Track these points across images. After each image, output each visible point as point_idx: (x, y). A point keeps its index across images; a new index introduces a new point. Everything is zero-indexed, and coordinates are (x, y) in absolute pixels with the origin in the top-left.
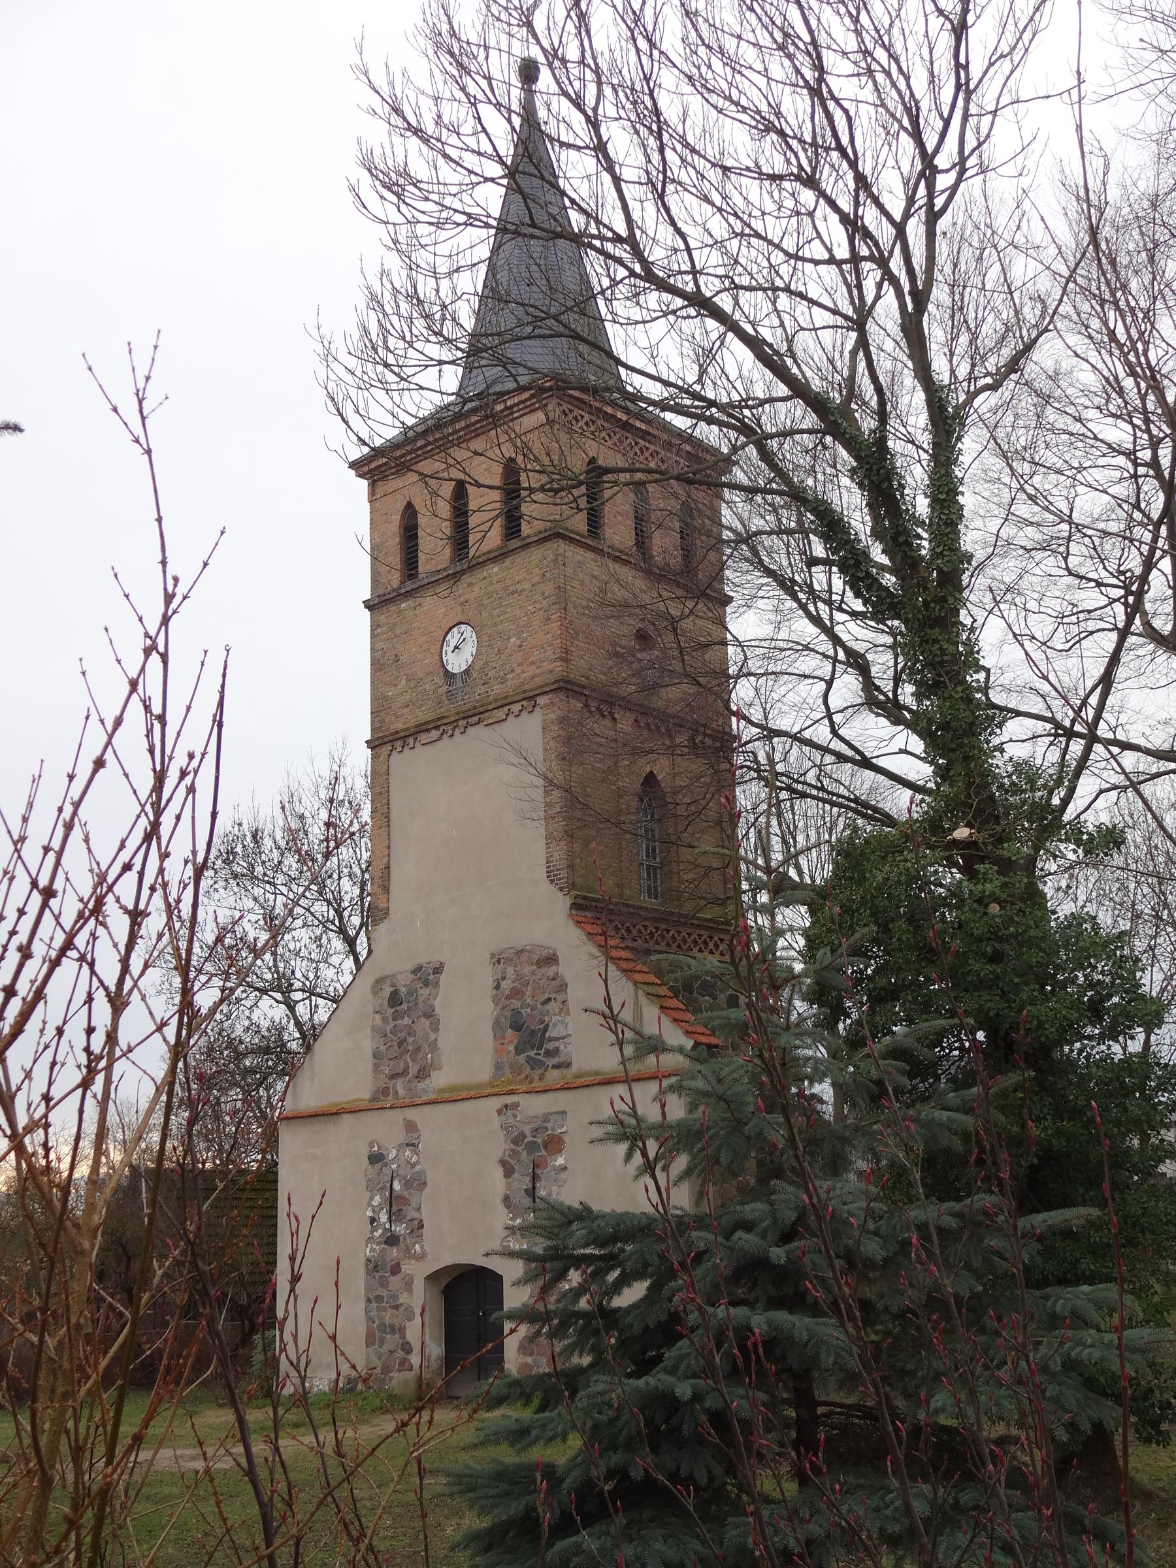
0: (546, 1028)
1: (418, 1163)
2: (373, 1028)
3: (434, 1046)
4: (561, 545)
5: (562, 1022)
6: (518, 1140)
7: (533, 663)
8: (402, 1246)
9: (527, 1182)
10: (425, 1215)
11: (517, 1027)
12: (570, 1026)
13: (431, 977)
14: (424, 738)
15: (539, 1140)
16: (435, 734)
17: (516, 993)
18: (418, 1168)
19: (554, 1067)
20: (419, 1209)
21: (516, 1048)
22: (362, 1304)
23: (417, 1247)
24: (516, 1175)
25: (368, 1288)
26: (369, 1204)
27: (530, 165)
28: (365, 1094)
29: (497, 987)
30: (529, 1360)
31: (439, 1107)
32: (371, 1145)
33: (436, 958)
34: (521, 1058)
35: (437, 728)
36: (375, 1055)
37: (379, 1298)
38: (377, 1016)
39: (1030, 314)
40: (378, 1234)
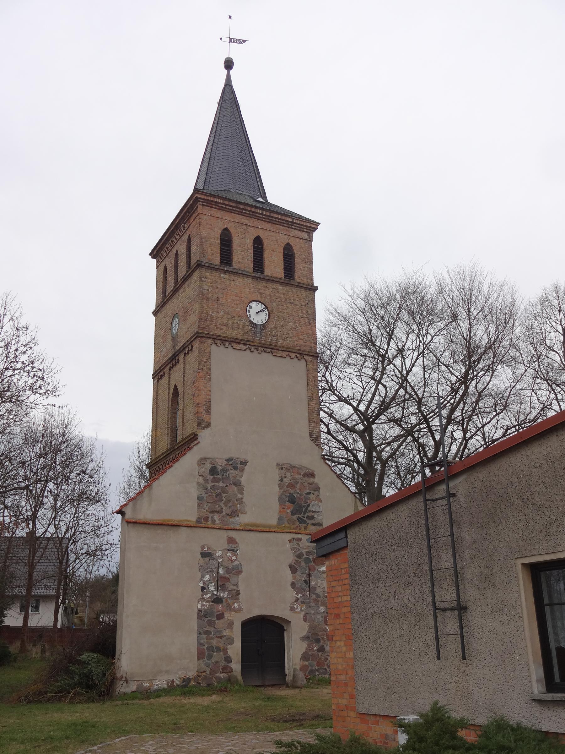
0: (309, 506)
1: (236, 560)
2: (198, 483)
3: (240, 501)
4: (203, 270)
5: (318, 505)
6: (299, 556)
7: (301, 339)
8: (225, 604)
9: (305, 577)
10: (241, 588)
11: (292, 500)
12: (321, 508)
13: (239, 466)
14: (236, 346)
15: (311, 558)
16: (243, 347)
17: (291, 486)
18: (236, 563)
19: (313, 524)
20: (237, 585)
21: (292, 512)
22: (195, 636)
23: (236, 605)
24: (298, 573)
25: (199, 626)
26: (201, 580)
27: (229, 102)
28: (193, 519)
29: (281, 480)
30: (307, 663)
31: (252, 534)
32: (203, 547)
33: (243, 457)
34: (295, 517)
35: (245, 344)
36: (199, 498)
37: (207, 633)
38: (201, 478)
39: (502, 317)
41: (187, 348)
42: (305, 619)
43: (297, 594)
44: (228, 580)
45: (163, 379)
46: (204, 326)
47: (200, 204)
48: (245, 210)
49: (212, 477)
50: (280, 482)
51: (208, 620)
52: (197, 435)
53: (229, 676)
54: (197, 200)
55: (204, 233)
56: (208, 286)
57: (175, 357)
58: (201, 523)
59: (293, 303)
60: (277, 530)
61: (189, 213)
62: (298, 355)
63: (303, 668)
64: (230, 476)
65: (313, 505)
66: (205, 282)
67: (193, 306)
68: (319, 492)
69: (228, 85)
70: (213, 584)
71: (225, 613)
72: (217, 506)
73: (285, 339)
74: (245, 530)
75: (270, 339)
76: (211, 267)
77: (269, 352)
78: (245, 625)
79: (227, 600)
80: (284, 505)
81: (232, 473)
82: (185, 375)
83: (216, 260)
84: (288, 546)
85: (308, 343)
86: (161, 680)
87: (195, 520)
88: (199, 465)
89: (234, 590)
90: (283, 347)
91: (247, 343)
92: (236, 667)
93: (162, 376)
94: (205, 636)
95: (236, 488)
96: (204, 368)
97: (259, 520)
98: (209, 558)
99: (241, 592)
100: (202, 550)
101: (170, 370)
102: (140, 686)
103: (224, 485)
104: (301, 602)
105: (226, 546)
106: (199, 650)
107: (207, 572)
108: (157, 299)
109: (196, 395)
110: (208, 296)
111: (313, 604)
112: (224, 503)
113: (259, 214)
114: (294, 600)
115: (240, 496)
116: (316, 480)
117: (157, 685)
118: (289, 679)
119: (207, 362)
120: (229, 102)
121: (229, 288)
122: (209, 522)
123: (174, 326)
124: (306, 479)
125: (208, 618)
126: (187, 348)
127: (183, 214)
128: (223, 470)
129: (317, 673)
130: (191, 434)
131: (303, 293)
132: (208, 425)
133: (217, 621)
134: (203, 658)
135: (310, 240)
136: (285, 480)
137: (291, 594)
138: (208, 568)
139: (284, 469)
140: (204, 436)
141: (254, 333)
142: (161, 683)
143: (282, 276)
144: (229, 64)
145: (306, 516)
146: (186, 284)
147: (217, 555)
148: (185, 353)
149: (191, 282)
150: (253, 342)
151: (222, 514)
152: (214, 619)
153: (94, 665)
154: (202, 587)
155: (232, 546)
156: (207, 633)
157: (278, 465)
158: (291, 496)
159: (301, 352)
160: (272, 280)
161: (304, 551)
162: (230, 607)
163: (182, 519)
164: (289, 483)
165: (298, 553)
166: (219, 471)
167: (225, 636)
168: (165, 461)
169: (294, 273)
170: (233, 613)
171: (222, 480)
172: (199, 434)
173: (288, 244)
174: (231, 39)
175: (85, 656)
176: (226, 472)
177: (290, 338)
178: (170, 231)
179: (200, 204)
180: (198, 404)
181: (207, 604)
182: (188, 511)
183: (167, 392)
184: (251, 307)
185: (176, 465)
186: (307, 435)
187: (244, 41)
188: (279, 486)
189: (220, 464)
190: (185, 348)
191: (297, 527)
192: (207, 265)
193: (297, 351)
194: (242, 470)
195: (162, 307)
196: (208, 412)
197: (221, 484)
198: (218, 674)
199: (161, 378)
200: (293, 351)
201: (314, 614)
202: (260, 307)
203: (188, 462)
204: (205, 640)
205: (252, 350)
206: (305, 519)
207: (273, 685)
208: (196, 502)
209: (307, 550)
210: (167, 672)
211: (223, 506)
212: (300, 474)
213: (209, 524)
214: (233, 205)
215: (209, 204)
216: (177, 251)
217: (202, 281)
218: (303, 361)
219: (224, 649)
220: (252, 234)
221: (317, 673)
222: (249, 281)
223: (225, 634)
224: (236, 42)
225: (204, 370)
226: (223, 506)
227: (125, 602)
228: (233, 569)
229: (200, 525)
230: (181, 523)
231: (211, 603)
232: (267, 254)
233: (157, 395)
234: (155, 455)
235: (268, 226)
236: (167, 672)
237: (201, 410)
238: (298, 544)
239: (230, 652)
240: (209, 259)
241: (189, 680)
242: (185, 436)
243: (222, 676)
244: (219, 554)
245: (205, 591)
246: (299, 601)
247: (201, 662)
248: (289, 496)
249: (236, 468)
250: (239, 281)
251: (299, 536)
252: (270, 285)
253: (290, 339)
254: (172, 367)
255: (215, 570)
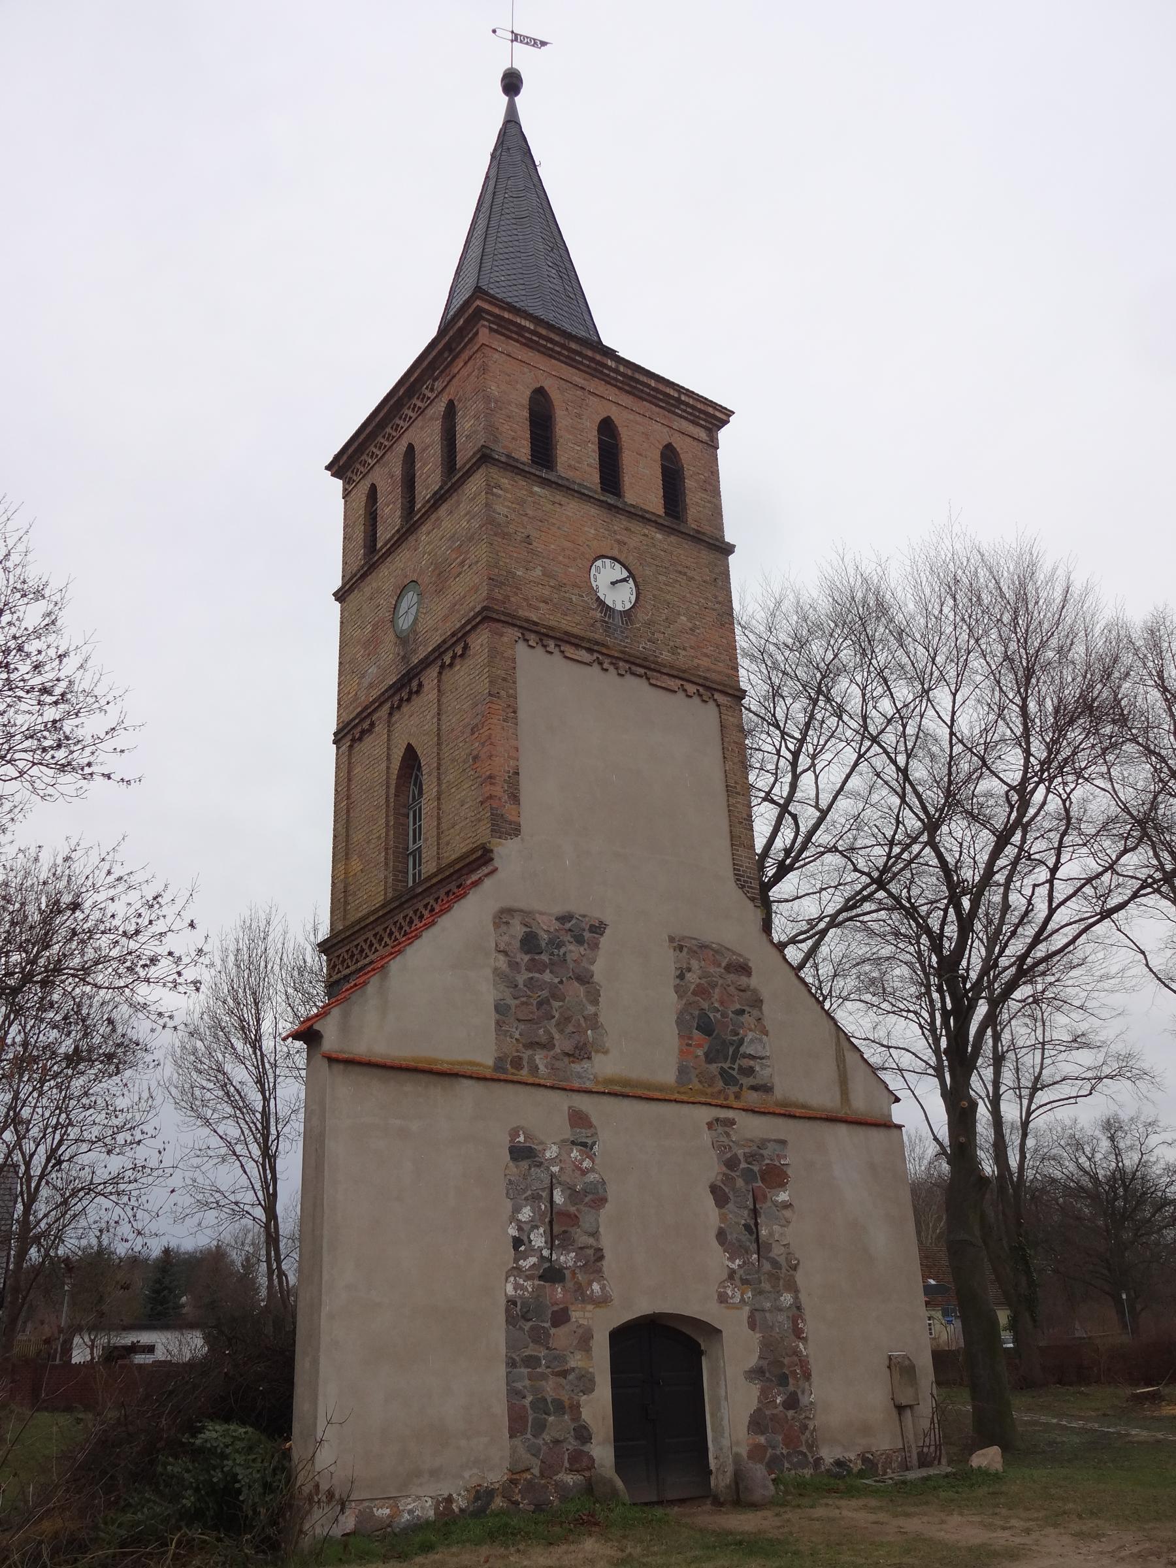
1: (592, 1170)
3: (593, 1022)
4: (494, 472)
5: (761, 1041)
6: (731, 1164)
8: (570, 1284)
9: (745, 1216)
10: (607, 1242)
11: (706, 1028)
13: (587, 935)
14: (570, 651)
15: (756, 1169)
16: (584, 655)
17: (701, 991)
18: (592, 1177)
19: (754, 1088)
20: (595, 1234)
21: (706, 1055)
22: (502, 1370)
23: (596, 1287)
24: (731, 1206)
25: (511, 1345)
26: (513, 1218)
27: (512, 153)
28: (486, 1058)
29: (681, 976)
30: (762, 1439)
31: (626, 1104)
32: (514, 1133)
33: (596, 914)
34: (714, 1068)
36: (497, 1008)
37: (531, 1362)
38: (501, 957)
40: (526, 1264)
41: (451, 650)
42: (752, 1325)
43: (732, 1259)
44: (574, 1219)
45: (368, 740)
46: (500, 597)
47: (484, 326)
48: (579, 354)
49: (526, 958)
50: (678, 981)
51: (532, 1328)
52: (492, 851)
53: (589, 1481)
54: (479, 313)
55: (494, 390)
56: (509, 507)
57: (410, 681)
58: (505, 1071)
59: (685, 574)
60: (676, 1096)
61: (451, 350)
62: (701, 690)
63: (756, 1452)
64: (568, 957)
65: (752, 1041)
66: (499, 496)
67: (467, 552)
68: (761, 1009)
69: (512, 121)
70: (541, 1230)
71: (572, 1308)
72: (541, 1031)
73: (674, 650)
74: (609, 1094)
75: (642, 647)
76: (511, 466)
77: (640, 676)
78: (618, 1336)
79: (574, 1273)
80: (690, 1038)
81: (573, 950)
82: (443, 717)
83: (523, 452)
84: (707, 1137)
85: (721, 667)
86: (419, 1498)
87: (490, 1062)
88: (496, 925)
89: (591, 1246)
90: (672, 667)
91: (596, 648)
92: (602, 1453)
93: (363, 732)
94: (525, 1371)
95: (582, 990)
96: (503, 693)
97: (637, 1073)
98: (529, 1162)
99: (606, 1253)
100: (512, 1141)
101: (390, 714)
102: (365, 1517)
103: (556, 980)
104: (741, 1279)
105: (567, 1134)
106: (511, 1408)
107: (526, 1199)
108: (345, 563)
109: (483, 755)
110: (506, 530)
111: (766, 1286)
112: (557, 1025)
113: (610, 368)
114: (725, 1276)
115: (591, 1009)
116: (754, 981)
117: (410, 1512)
118: (720, 1481)
119: (509, 679)
120: (512, 153)
121: (551, 520)
122: (525, 1072)
123: (402, 611)
124: (732, 977)
125: (532, 1322)
126: (451, 650)
127: (434, 353)
128: (551, 942)
129: (787, 1465)
130: (473, 851)
131: (706, 556)
132: (516, 831)
133: (553, 1331)
134: (523, 1432)
135: (714, 446)
136: (688, 975)
137: (718, 1261)
138: (524, 1191)
139: (685, 950)
140: (506, 852)
141: (607, 628)
142: (419, 1505)
143: (661, 512)
144: (512, 83)
145: (736, 1066)
146: (443, 510)
147: (548, 1155)
148: (442, 667)
149: (458, 503)
150: (607, 647)
151: (552, 1053)
152: (546, 1325)
153: (240, 1459)
154: (514, 1238)
155: (582, 1134)
156: (531, 1362)
157: (672, 939)
158: (703, 1015)
159: (708, 684)
160: (638, 515)
161: (740, 1152)
162: (583, 1294)
163: (460, 1059)
164: (697, 986)
165: (729, 1155)
166: (543, 944)
167: (573, 1369)
168: (379, 929)
169: (685, 509)
170: (590, 1307)
171: (548, 964)
172: (495, 849)
173: (670, 444)
174: (516, 35)
175: (213, 1433)
176: (559, 947)
177: (684, 649)
178: (392, 402)
179: (484, 326)
180: (490, 777)
181: (528, 1285)
182: (473, 1039)
183: (384, 765)
184: (598, 570)
185: (445, 921)
186: (729, 873)
187: (544, 44)
188: (677, 989)
189: (546, 926)
190: (441, 654)
191: (720, 1092)
192: (503, 459)
193: (701, 681)
194: (595, 946)
195: (364, 576)
196: (515, 798)
197: (547, 976)
198: (560, 1475)
199: (360, 739)
200: (694, 679)
201: (770, 1311)
202: (619, 572)
203: (469, 918)
204: (527, 1383)
205: (606, 666)
206: (734, 1073)
207: (682, 1501)
208: (493, 1017)
209: (747, 1150)
210: (435, 1473)
211: (554, 1031)
212: (719, 966)
213: (524, 1074)
214: (557, 338)
215: (503, 328)
216: (411, 448)
217: (493, 494)
218: (712, 704)
219: (571, 1407)
220: (596, 411)
221: (787, 1465)
222: (593, 511)
223: (573, 1364)
224: (527, 43)
225: (502, 696)
226: (554, 1031)
227: (325, 1277)
228: (585, 1192)
229: (503, 1077)
230: (456, 1069)
231: (537, 1282)
232: (628, 459)
233: (349, 780)
234: (344, 919)
235: (626, 400)
236: (435, 1473)
237: (498, 790)
238: (728, 1134)
239: (586, 1415)
240: (504, 447)
241: (490, 1494)
242: (444, 863)
243: (569, 1479)
244: (552, 1152)
245: (522, 1248)
246: (737, 1277)
247: (517, 1441)
248: (700, 1017)
249: (579, 940)
250: (573, 509)
251: (730, 1114)
252: (636, 526)
253: (683, 653)
254: (399, 707)
255: (544, 1194)
